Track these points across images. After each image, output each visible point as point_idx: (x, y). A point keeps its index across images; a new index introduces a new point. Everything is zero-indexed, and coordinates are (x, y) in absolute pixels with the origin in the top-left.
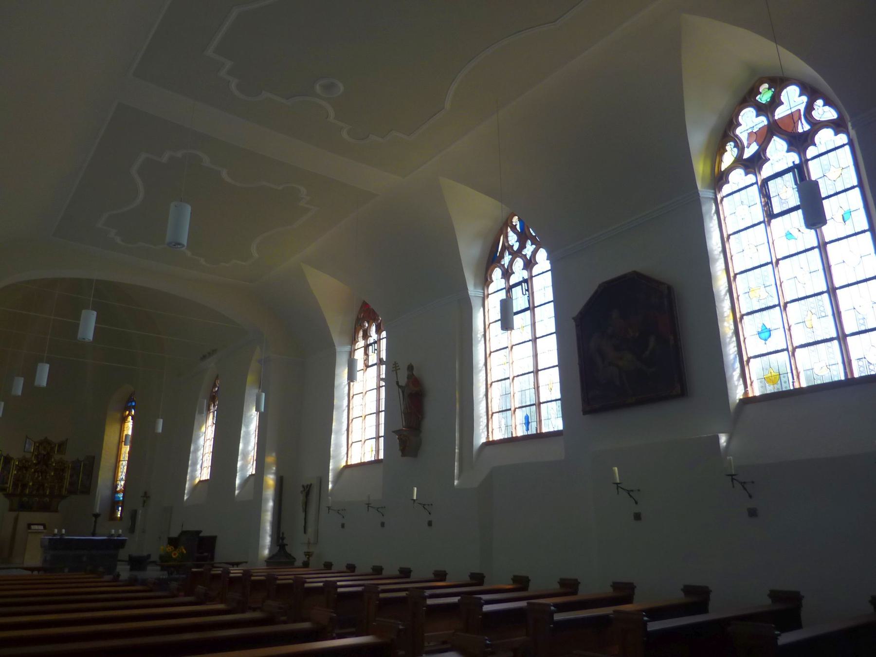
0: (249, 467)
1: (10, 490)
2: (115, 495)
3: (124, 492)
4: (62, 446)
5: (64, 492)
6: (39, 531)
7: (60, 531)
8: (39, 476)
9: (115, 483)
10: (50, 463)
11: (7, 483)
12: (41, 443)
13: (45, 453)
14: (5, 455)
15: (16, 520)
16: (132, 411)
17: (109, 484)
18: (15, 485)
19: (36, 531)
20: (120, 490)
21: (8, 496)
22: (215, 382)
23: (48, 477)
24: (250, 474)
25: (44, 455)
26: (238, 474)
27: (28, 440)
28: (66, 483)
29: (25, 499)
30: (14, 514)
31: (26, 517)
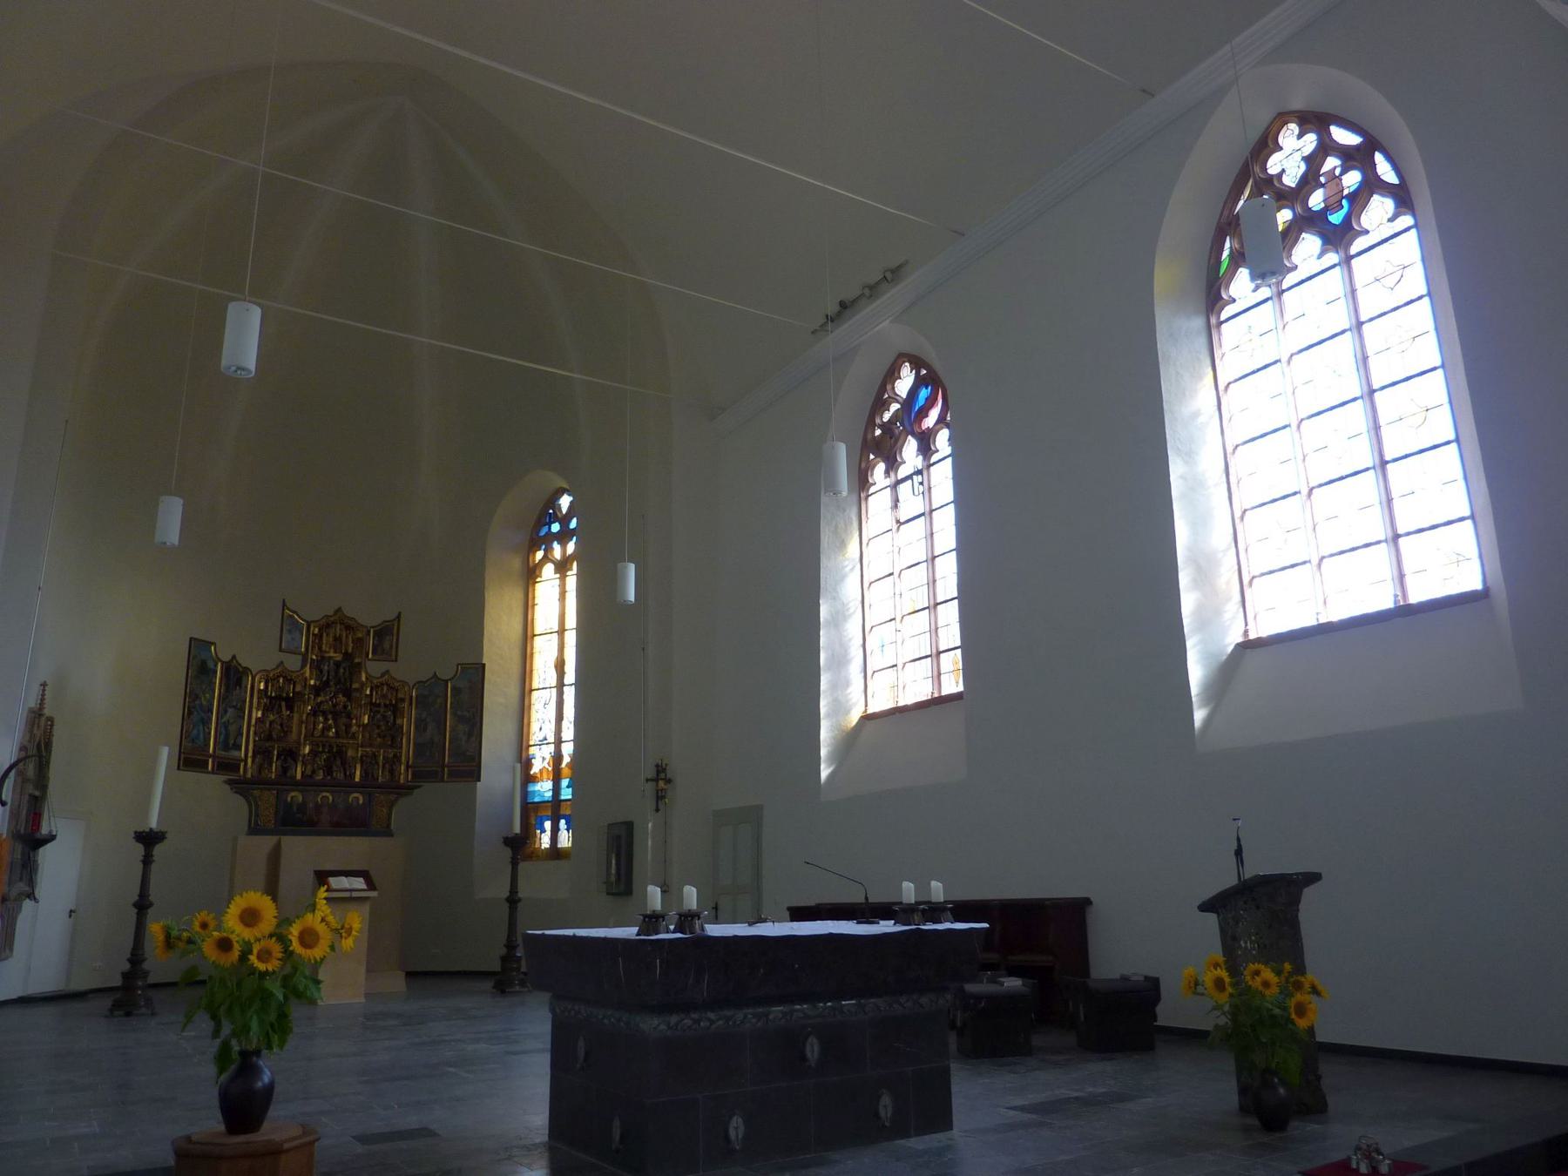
0: (1227, 616)
1: (249, 768)
4: (386, 633)
5: (403, 775)
6: (355, 894)
7: (923, 886)
8: (327, 728)
10: (356, 686)
12: (326, 626)
13: (338, 657)
14: (226, 658)
15: (275, 857)
16: (552, 549)
17: (509, 754)
18: (262, 752)
19: (347, 895)
20: (541, 771)
21: (241, 786)
23: (354, 729)
24: (1240, 640)
25: (338, 664)
26: (1189, 644)
28: (407, 750)
29: (296, 796)
30: (268, 842)
31: (302, 852)
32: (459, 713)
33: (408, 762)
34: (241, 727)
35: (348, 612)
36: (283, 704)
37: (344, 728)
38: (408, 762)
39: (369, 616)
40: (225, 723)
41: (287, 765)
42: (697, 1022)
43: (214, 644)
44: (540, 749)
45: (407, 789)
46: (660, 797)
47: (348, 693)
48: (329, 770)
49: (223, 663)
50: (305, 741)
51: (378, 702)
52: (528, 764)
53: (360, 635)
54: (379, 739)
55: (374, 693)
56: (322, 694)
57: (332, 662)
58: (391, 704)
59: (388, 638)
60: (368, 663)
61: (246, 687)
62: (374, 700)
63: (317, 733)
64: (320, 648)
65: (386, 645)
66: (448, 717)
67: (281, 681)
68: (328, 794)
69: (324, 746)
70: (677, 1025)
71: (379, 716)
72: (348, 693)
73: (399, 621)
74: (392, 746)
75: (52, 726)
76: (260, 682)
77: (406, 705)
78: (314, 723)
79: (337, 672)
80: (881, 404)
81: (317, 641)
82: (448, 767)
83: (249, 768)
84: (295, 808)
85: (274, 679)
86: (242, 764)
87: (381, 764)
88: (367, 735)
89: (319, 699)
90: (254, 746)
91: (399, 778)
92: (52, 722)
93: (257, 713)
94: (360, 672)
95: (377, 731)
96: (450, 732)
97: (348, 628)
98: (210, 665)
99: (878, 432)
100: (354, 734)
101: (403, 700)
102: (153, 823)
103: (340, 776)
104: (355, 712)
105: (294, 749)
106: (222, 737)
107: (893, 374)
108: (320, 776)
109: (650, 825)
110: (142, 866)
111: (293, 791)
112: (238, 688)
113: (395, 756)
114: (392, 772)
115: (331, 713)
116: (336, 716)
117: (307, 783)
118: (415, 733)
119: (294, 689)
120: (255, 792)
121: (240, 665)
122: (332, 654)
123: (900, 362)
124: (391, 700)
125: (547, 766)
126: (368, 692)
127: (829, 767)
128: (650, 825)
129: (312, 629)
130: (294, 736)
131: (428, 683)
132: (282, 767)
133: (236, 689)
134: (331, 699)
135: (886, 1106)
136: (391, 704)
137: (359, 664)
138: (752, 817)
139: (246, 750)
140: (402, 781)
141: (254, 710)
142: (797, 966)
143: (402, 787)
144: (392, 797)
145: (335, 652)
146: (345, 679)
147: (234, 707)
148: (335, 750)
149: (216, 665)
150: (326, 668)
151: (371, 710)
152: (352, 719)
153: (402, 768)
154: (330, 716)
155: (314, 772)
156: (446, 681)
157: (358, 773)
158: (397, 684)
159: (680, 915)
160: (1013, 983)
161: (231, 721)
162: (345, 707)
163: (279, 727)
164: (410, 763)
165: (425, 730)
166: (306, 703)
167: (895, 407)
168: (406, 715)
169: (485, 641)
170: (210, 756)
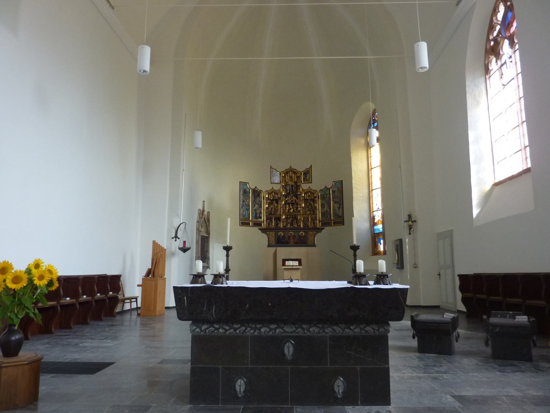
2: (374, 227)
3: (383, 223)
4: (307, 173)
6: (294, 267)
9: (372, 215)
10: (298, 193)
11: (261, 218)
12: (286, 172)
15: (275, 254)
17: (366, 215)
18: (269, 219)
19: (291, 267)
20: (378, 221)
21: (263, 231)
22: (492, 20)
23: (299, 209)
25: (292, 186)
27: (272, 169)
28: (319, 216)
29: (281, 233)
30: (273, 249)
31: (283, 252)
32: (335, 200)
33: (319, 219)
34: (261, 211)
35: (293, 167)
36: (275, 201)
37: (295, 209)
38: (319, 219)
39: (301, 168)
40: (255, 210)
41: (278, 223)
42: (218, 329)
43: (248, 183)
44: (377, 212)
45: (320, 230)
46: (410, 227)
47: (296, 196)
48: (292, 224)
49: (252, 189)
50: (283, 214)
51: (307, 198)
52: (374, 218)
53: (298, 175)
54: (308, 212)
55: (306, 195)
56: (288, 197)
57: (290, 186)
58: (312, 199)
59: (308, 175)
60: (302, 185)
61: (262, 197)
62: (306, 198)
63: (286, 211)
64: (285, 181)
65: (308, 178)
66: (331, 202)
67: (273, 194)
68: (292, 232)
69: (290, 216)
70: (206, 329)
71: (308, 204)
72: (296, 196)
73: (311, 168)
74: (313, 214)
75: (209, 214)
76: (266, 195)
77: (317, 199)
78: (285, 208)
79: (292, 189)
80: (491, 28)
81: (284, 178)
82: (333, 220)
83: (264, 225)
84: (281, 238)
85: (271, 193)
86: (263, 223)
87: (310, 221)
88: (304, 211)
89: (287, 199)
90: (266, 217)
91: (317, 225)
92: (209, 213)
93: (266, 206)
94: (300, 188)
95: (307, 209)
96: (333, 207)
97: (294, 173)
98: (248, 190)
99: (492, 43)
100: (299, 210)
101: (316, 197)
102: (228, 244)
103: (296, 226)
104: (299, 202)
105: (279, 217)
106: (254, 214)
107: (495, 11)
108: (289, 226)
109: (407, 240)
110: (226, 257)
111: (280, 232)
112: (258, 197)
113: (315, 217)
114: (314, 223)
115: (291, 204)
116: (293, 204)
117: (285, 229)
118: (321, 209)
119: (278, 196)
120: (268, 232)
121: (258, 190)
122: (290, 183)
123: (498, 3)
124: (312, 197)
125: (380, 219)
126: (303, 195)
127: (477, 209)
128: (407, 240)
129: (281, 175)
130: (279, 213)
131: (324, 190)
132: (276, 223)
133: (258, 198)
134: (291, 199)
135: (339, 386)
136: (312, 199)
137: (299, 185)
138: (449, 235)
139: (264, 217)
140: (318, 227)
141: (265, 205)
142: (270, 304)
143: (319, 229)
144: (315, 232)
145: (291, 182)
146: (295, 191)
147: (258, 204)
148: (294, 217)
149: (250, 190)
150: (288, 188)
151: (305, 202)
152: (298, 205)
153: (318, 221)
154: (290, 205)
155: (286, 225)
156: (330, 189)
157: (302, 224)
158: (313, 191)
159: (378, 275)
160: (522, 319)
161: (257, 209)
162: (296, 201)
163: (274, 210)
164: (320, 220)
165: (324, 208)
166: (282, 201)
167: (498, 27)
168: (317, 202)
169: (353, 173)
170: (251, 221)
